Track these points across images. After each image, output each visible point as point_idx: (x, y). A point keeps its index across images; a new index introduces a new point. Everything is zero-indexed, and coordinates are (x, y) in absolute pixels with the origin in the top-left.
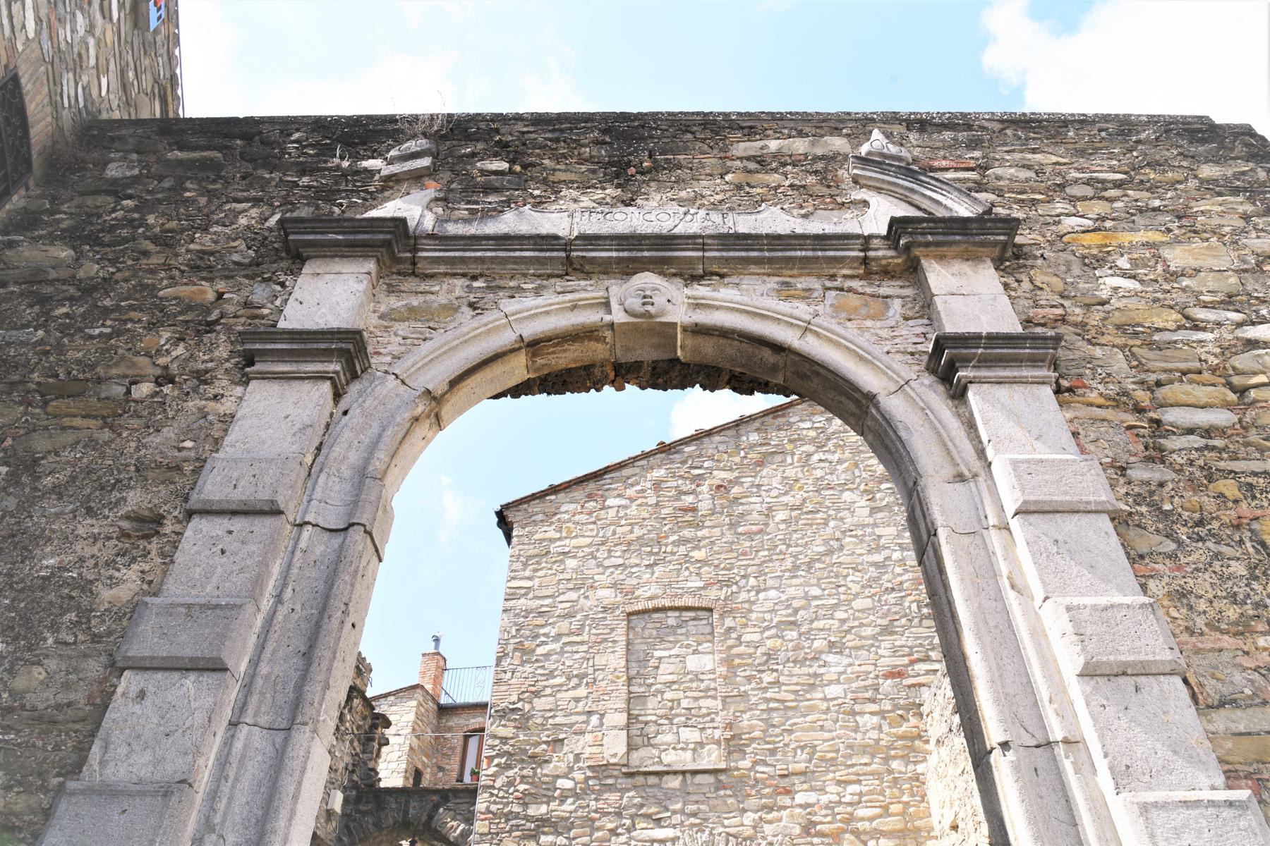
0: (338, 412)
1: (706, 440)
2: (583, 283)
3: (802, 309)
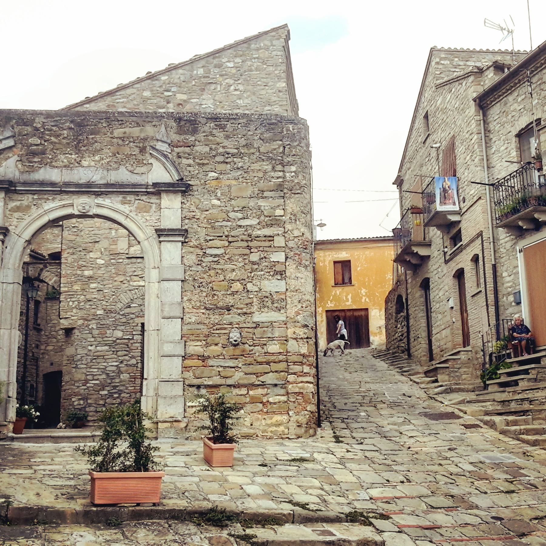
0: (4, 247)
1: (174, 72)
2: (66, 197)
3: (126, 208)
